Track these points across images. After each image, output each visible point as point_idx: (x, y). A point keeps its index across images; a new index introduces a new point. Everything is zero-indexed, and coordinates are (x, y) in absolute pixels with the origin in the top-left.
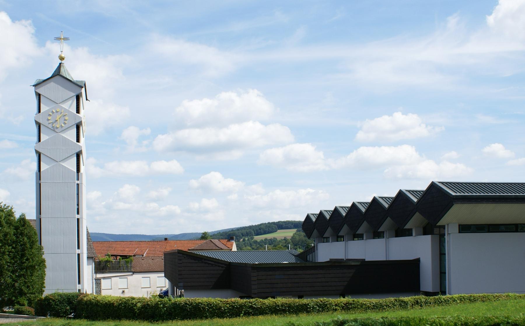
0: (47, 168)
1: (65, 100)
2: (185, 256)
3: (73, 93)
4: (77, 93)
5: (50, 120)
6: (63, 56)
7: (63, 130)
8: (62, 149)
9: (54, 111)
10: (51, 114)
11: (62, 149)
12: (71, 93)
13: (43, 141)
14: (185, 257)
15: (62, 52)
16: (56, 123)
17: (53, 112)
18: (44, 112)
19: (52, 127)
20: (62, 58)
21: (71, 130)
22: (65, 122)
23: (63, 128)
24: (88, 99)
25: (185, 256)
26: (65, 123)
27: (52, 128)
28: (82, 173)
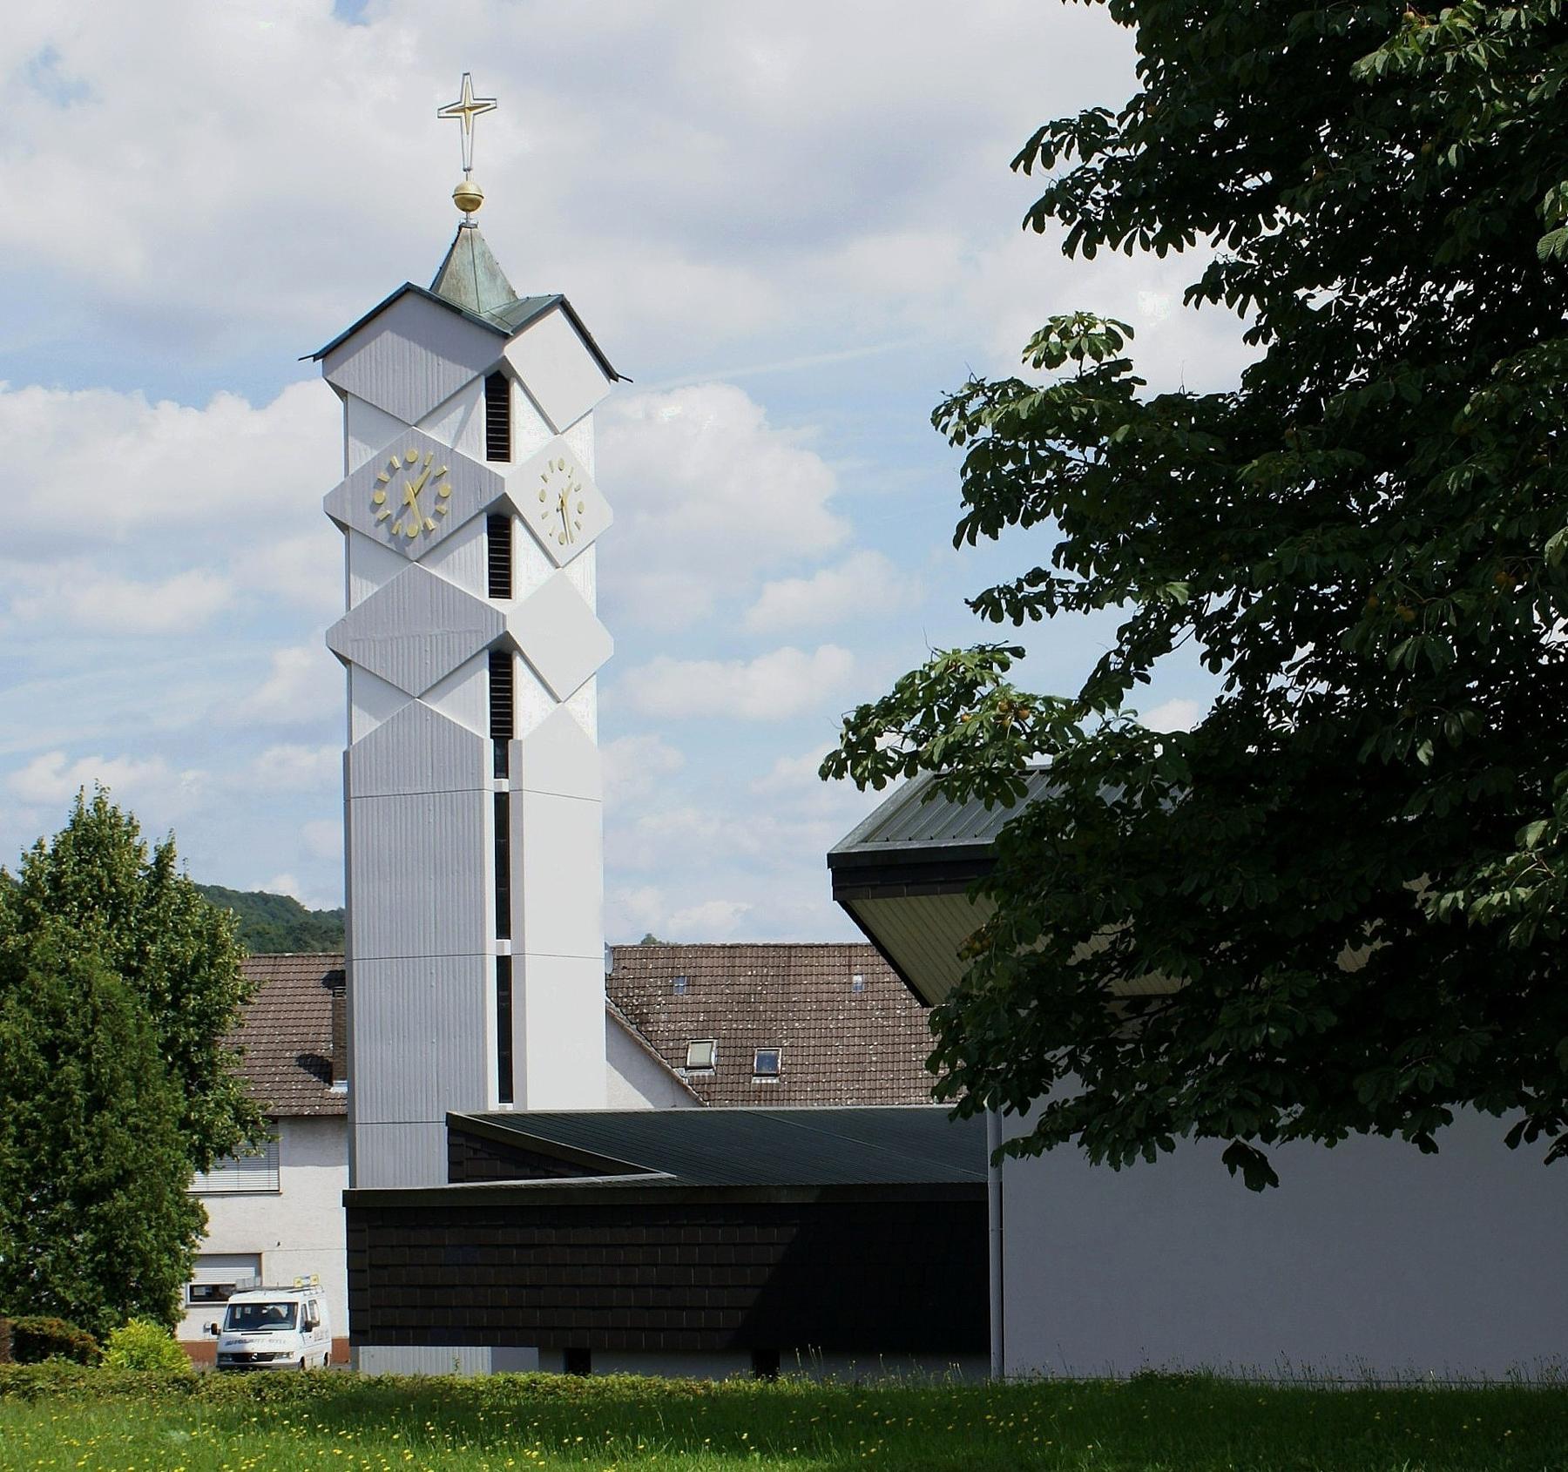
0: (374, 728)
1: (441, 405)
2: (478, 1146)
3: (470, 372)
4: (488, 363)
5: (383, 507)
6: (471, 189)
7: (436, 547)
8: (431, 636)
9: (398, 464)
10: (385, 476)
11: (431, 636)
12: (463, 369)
13: (359, 607)
14: (475, 1151)
15: (469, 170)
16: (405, 517)
17: (392, 469)
18: (357, 471)
19: (388, 536)
20: (468, 203)
21: (465, 543)
22: (438, 507)
23: (435, 538)
24: (617, 370)
25: (478, 1146)
26: (438, 515)
27: (390, 541)
28: (520, 742)
